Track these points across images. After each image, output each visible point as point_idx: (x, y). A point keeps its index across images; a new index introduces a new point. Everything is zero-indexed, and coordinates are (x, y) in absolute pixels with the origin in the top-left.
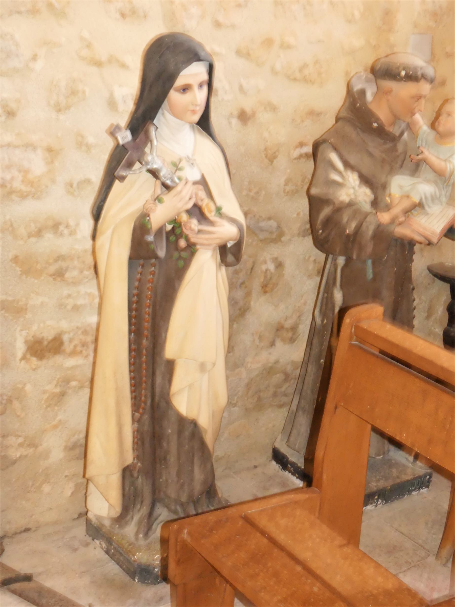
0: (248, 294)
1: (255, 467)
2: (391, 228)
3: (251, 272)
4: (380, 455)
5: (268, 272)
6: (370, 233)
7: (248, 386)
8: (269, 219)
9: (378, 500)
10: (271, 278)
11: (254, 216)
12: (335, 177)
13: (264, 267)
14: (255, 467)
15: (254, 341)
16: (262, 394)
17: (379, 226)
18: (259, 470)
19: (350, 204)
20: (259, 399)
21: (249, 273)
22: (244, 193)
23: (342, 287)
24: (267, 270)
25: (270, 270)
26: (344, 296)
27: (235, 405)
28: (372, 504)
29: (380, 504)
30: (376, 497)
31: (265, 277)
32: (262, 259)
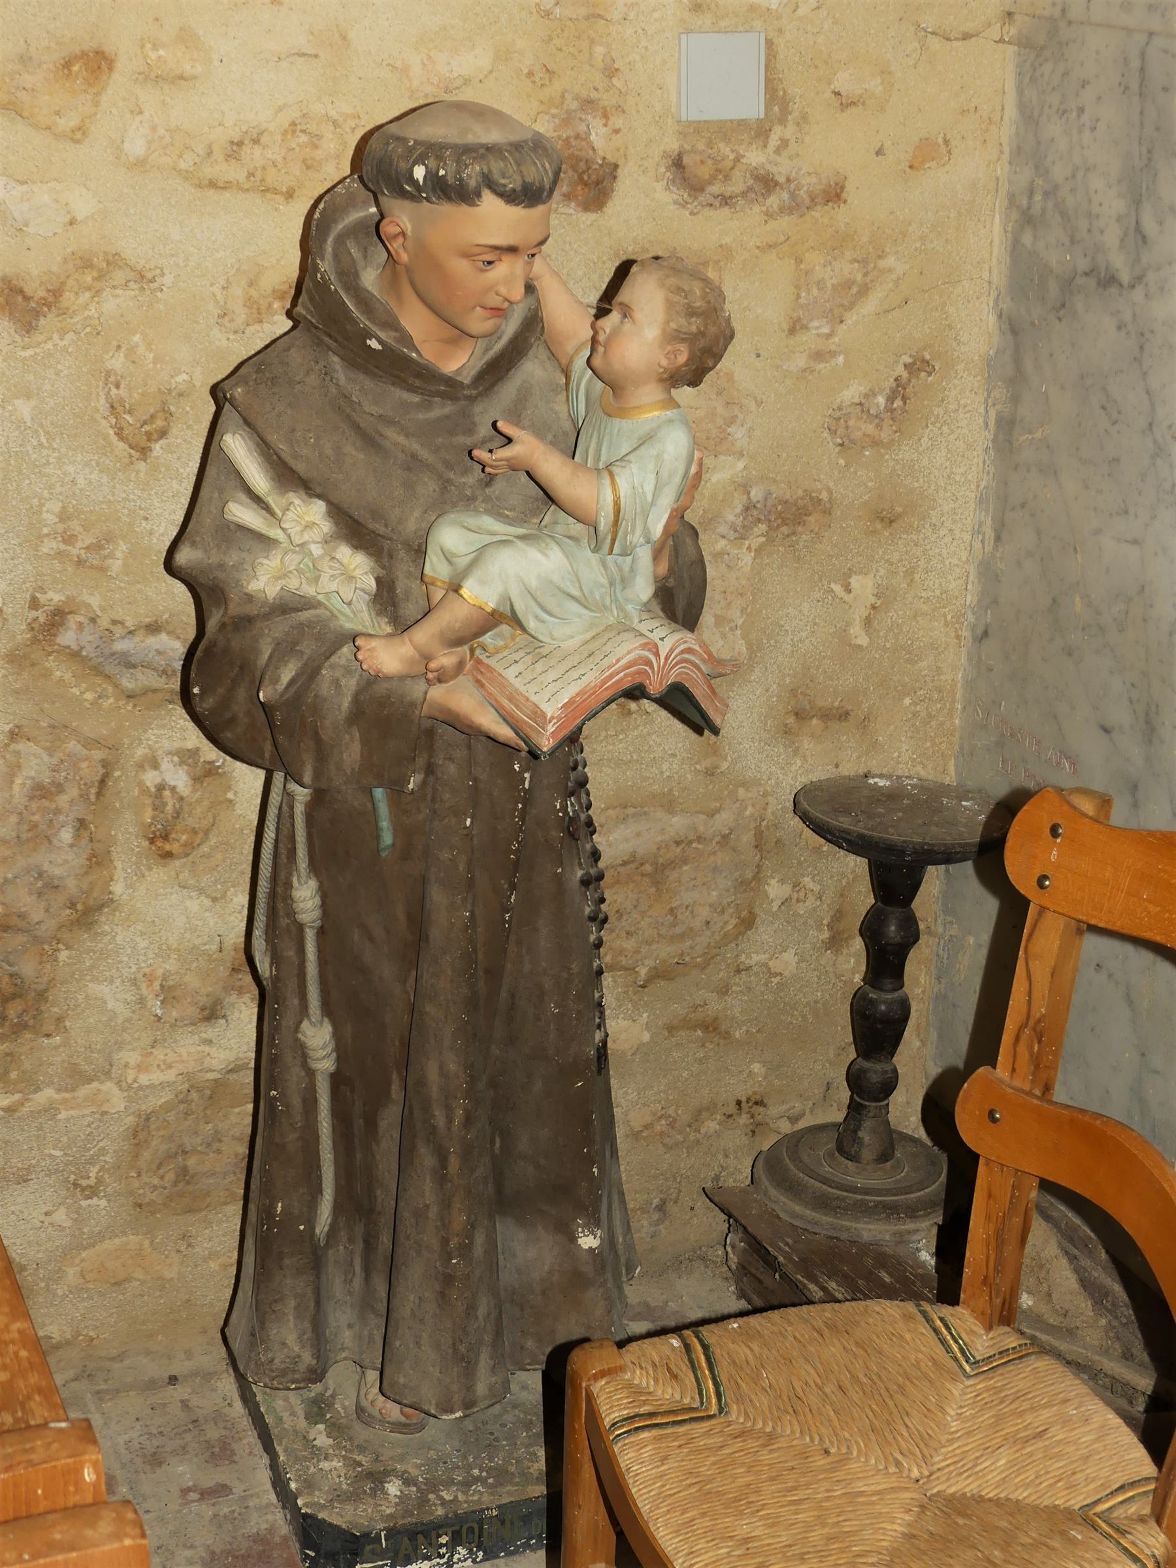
0: (99, 860)
1: (173, 1380)
2: (417, 689)
3: (99, 794)
4: (452, 1412)
5: (167, 793)
6: (346, 703)
7: (139, 1135)
8: (153, 628)
9: (452, 1546)
10: (178, 814)
11: (93, 620)
12: (242, 513)
13: (151, 778)
14: (173, 1380)
15: (142, 1001)
16: (191, 1162)
17: (372, 680)
18: (179, 1392)
19: (286, 606)
20: (184, 1174)
21: (93, 798)
22: (50, 546)
23: (314, 867)
24: (161, 788)
25: (173, 789)
26: (324, 894)
27: (92, 1192)
28: (428, 1558)
29: (465, 1560)
30: (444, 1540)
31: (158, 807)
32: (140, 752)
